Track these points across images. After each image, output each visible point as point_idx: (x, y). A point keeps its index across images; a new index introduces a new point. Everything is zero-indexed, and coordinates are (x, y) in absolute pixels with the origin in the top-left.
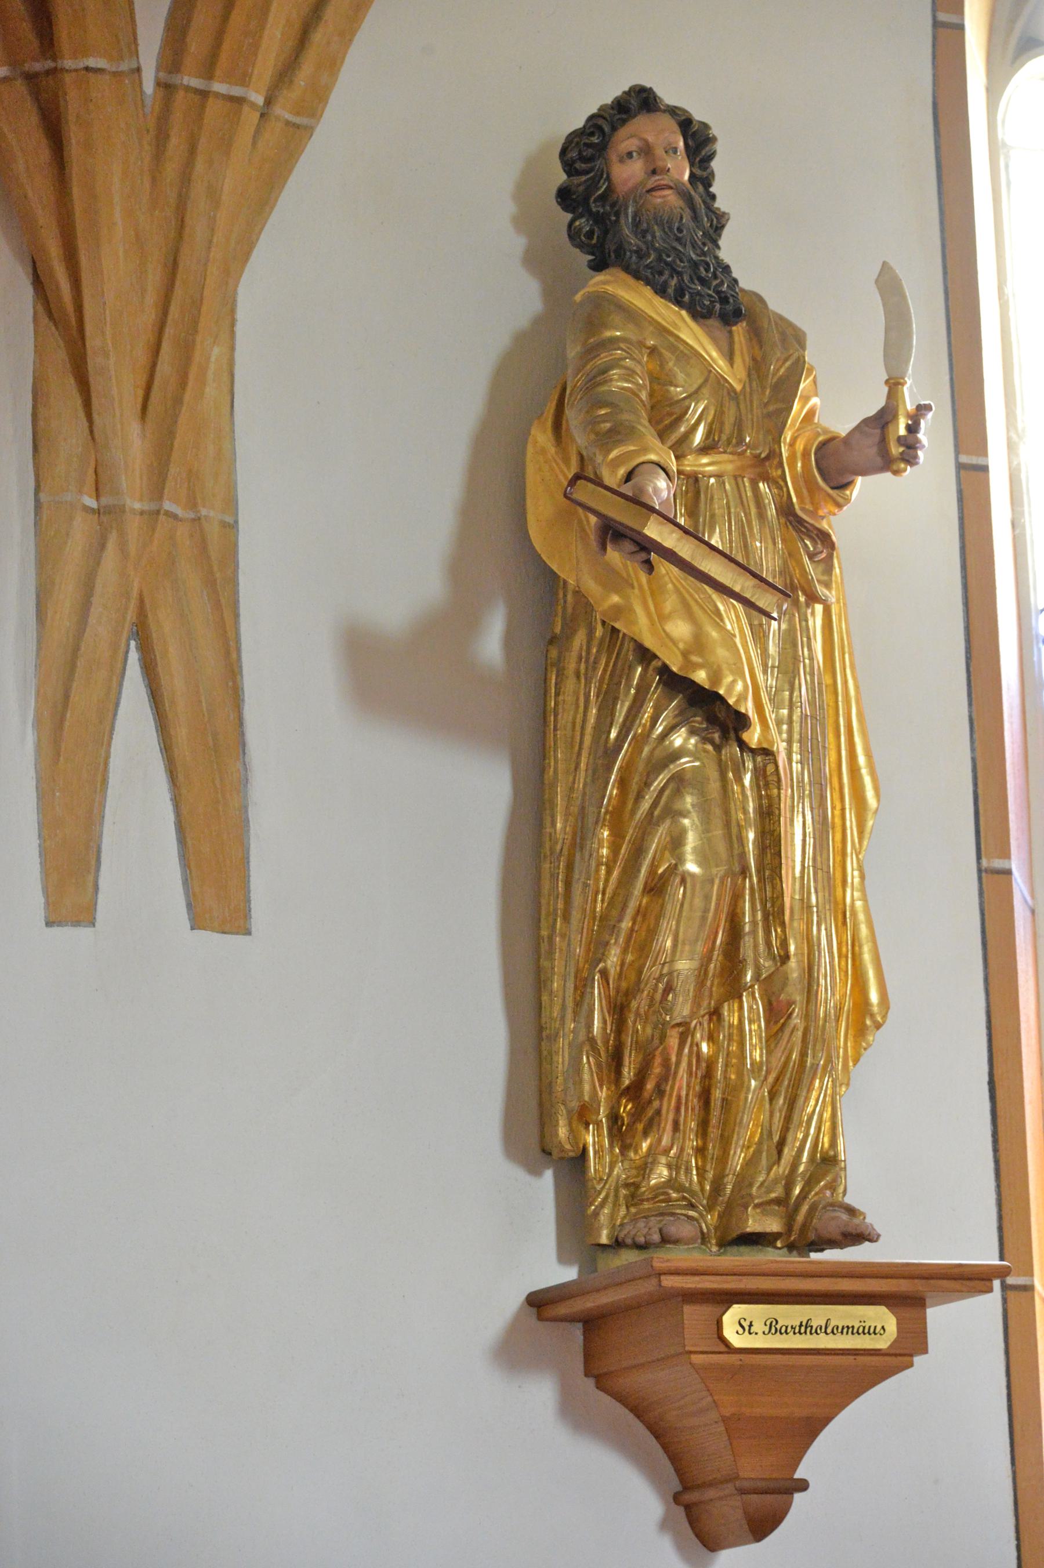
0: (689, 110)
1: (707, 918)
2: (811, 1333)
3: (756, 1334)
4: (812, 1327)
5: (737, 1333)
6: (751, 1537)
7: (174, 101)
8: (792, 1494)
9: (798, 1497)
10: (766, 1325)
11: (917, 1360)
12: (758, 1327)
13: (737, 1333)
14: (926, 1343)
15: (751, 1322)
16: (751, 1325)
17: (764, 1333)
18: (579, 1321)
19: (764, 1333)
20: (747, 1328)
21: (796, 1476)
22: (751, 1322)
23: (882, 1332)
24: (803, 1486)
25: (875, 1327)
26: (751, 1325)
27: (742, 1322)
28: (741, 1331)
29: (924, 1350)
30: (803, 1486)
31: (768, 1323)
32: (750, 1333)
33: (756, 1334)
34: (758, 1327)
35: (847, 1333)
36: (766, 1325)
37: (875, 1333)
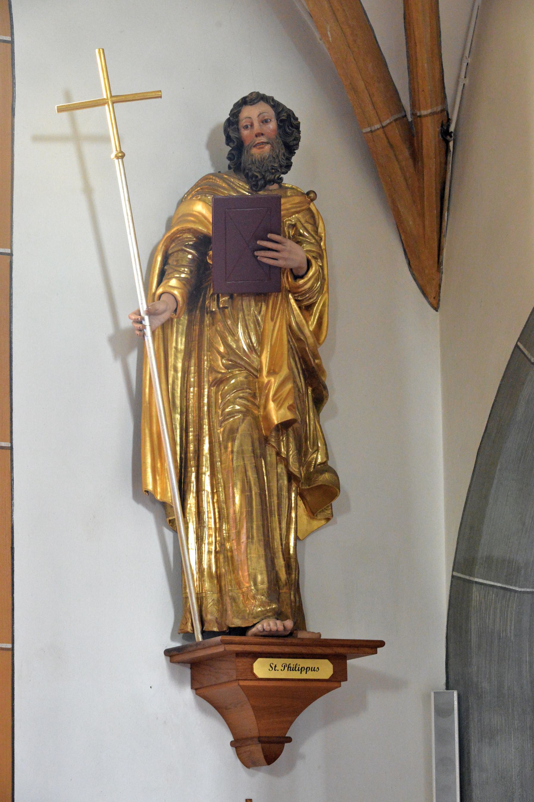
0: (292, 110)
1: (219, 355)
2: (312, 671)
3: (278, 670)
4: (291, 667)
5: (269, 670)
6: (266, 764)
7: (339, 653)
8: (284, 744)
9: (286, 745)
10: (282, 666)
11: (343, 683)
12: (279, 667)
13: (269, 670)
14: (347, 678)
15: (276, 665)
16: (275, 666)
17: (281, 670)
18: (189, 663)
19: (281, 670)
20: (274, 668)
21: (287, 736)
22: (276, 665)
23: (317, 670)
24: (289, 740)
25: (314, 668)
26: (275, 666)
27: (272, 665)
28: (271, 669)
29: (345, 679)
30: (289, 740)
31: (283, 665)
32: (275, 670)
33: (278, 670)
34: (279, 667)
35: (312, 668)
36: (282, 666)
37: (314, 671)
